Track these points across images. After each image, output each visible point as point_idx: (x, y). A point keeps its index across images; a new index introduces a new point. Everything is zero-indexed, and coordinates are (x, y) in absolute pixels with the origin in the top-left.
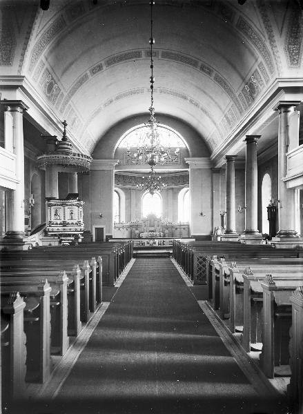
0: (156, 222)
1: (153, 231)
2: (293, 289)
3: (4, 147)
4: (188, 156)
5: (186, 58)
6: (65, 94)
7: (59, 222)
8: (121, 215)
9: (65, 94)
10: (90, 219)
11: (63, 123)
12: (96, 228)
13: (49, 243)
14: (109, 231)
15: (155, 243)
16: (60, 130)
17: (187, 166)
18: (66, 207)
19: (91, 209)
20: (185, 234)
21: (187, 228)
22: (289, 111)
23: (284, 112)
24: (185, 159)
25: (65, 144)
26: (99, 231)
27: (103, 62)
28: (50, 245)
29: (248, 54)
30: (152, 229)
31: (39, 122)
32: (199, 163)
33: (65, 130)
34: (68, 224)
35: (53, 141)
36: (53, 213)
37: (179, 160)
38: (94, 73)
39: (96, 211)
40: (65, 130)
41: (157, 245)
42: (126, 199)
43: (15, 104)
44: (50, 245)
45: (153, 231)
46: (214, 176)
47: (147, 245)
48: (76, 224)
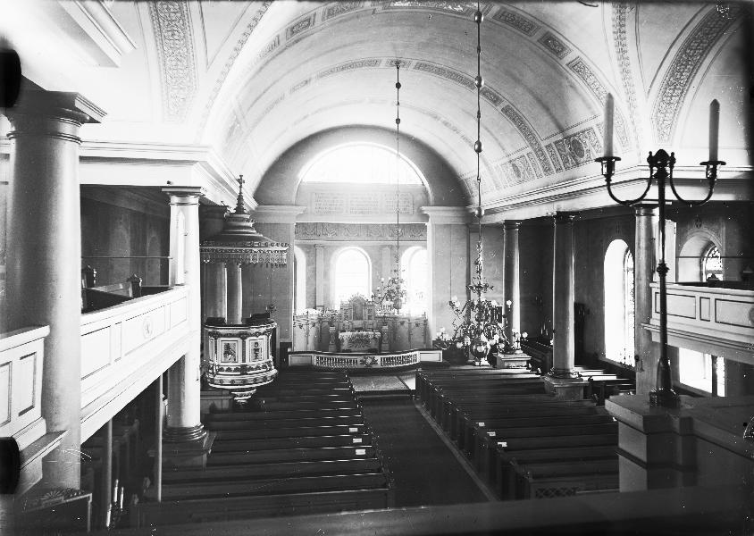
0: (365, 312)
1: (359, 329)
4: (427, 204)
5: (457, 75)
7: (232, 365)
11: (238, 180)
13: (212, 402)
15: (374, 362)
16: (231, 190)
17: (426, 217)
20: (417, 337)
21: (424, 325)
22: (653, 215)
23: (645, 215)
24: (424, 208)
29: (570, 93)
30: (358, 323)
32: (440, 216)
33: (241, 193)
34: (251, 369)
35: (217, 215)
36: (221, 349)
37: (411, 208)
40: (241, 193)
41: (379, 365)
42: (308, 265)
43: (183, 193)
45: (359, 329)
46: (471, 238)
47: (359, 366)
48: (264, 367)
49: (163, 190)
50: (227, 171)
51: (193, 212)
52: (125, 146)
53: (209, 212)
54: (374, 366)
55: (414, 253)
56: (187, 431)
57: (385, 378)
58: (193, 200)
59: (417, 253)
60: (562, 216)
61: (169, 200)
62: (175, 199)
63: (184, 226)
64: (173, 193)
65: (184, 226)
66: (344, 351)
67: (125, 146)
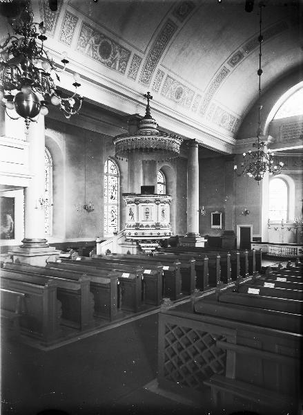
2: (297, 158)
3: (46, 136)
6: (203, 95)
8: (290, 209)
9: (203, 95)
10: (233, 216)
12: (242, 228)
14: (258, 230)
18: (140, 205)
19: (235, 203)
25: (148, 123)
26: (246, 232)
27: (241, 50)
28: (129, 253)
31: (100, 102)
34: (142, 226)
38: (234, 64)
39: (241, 206)
44: (129, 253)
48: (153, 226)
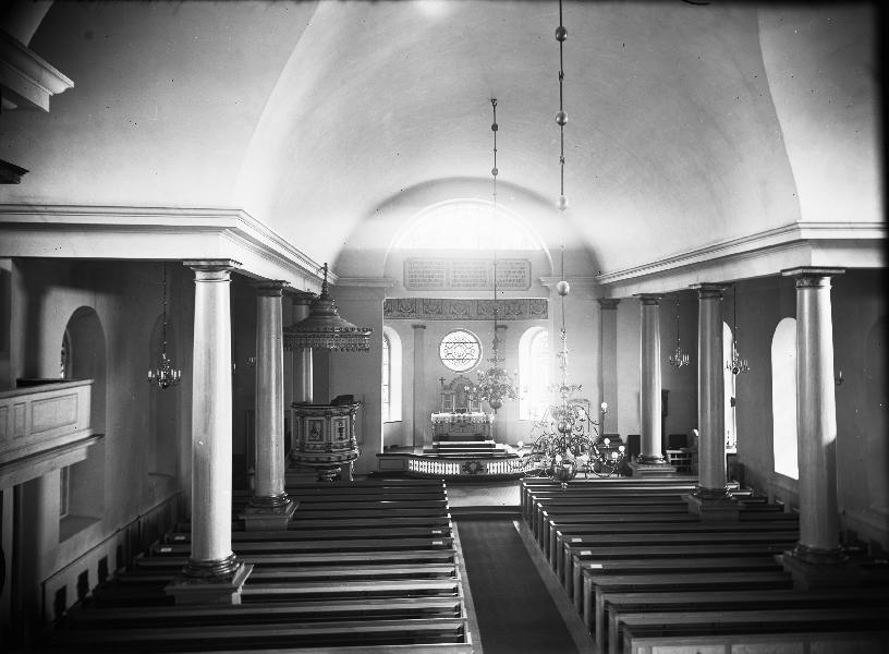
43: (213, 266)
49: (185, 263)
50: (273, 236)
51: (223, 290)
52: (12, 208)
53: (247, 292)
54: (479, 473)
55: (538, 332)
56: (217, 564)
57: (340, 568)
58: (224, 275)
59: (539, 336)
60: (707, 289)
61: (194, 276)
62: (199, 275)
63: (213, 306)
64: (199, 267)
65: (213, 306)
66: (828, 275)
67: (12, 208)
